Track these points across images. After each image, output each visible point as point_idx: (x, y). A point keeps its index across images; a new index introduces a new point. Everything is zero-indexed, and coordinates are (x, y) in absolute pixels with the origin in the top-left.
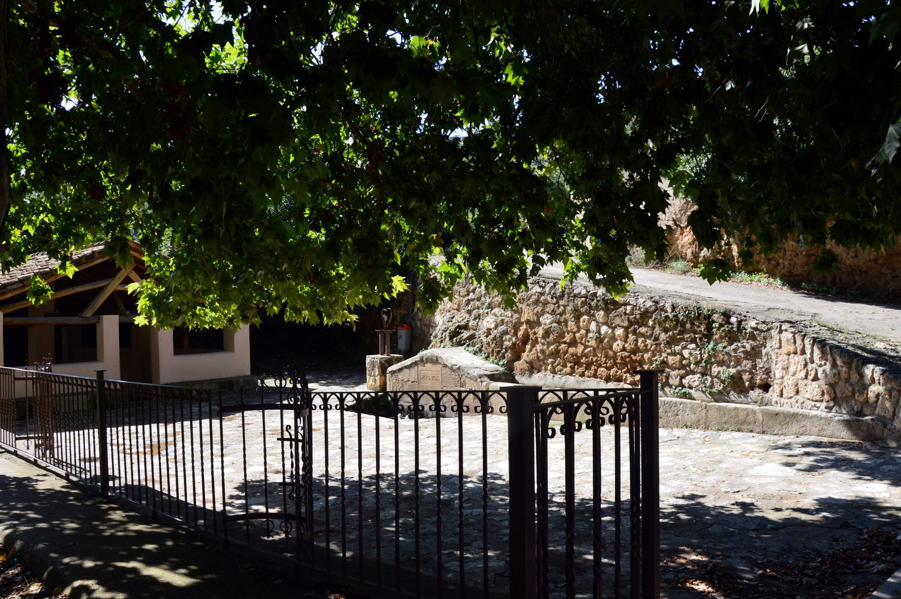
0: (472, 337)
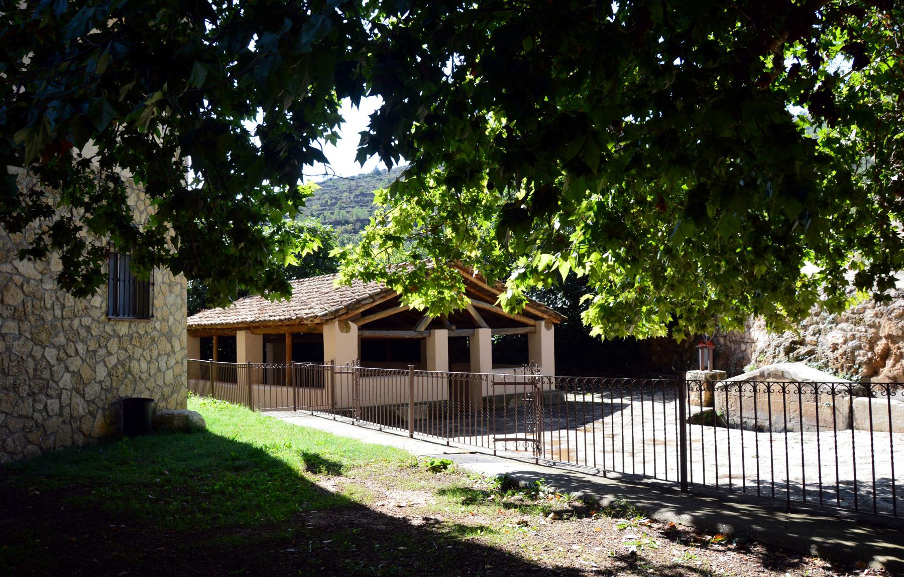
0: (811, 353)
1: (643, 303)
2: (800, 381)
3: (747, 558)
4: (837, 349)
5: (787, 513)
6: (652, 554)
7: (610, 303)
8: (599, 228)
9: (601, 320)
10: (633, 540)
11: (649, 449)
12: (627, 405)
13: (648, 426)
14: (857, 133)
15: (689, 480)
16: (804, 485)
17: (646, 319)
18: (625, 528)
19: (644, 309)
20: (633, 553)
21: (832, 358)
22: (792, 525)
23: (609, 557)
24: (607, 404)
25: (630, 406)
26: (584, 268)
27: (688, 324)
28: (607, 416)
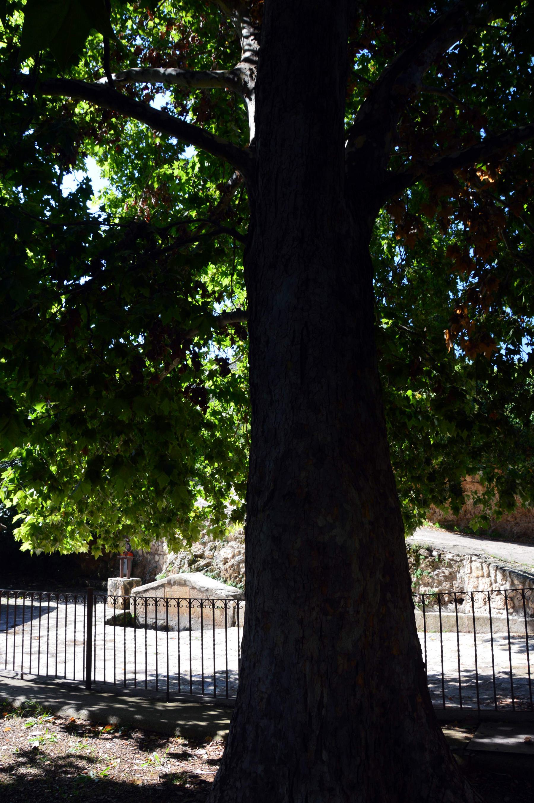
0: (208, 565)
1: (68, 524)
2: (178, 597)
3: (128, 743)
4: (228, 562)
5: (165, 702)
6: (51, 748)
7: (39, 523)
8: (27, 470)
9: (31, 537)
10: (37, 737)
11: (70, 650)
12: (53, 609)
13: (70, 628)
14: (234, 409)
15: (93, 678)
16: (191, 676)
17: (70, 537)
18: (32, 726)
19: (69, 528)
20: (36, 748)
21: (223, 569)
22: (167, 712)
23: (14, 754)
24: (37, 607)
25: (56, 610)
26: (11, 500)
27: (105, 543)
28: (35, 619)
